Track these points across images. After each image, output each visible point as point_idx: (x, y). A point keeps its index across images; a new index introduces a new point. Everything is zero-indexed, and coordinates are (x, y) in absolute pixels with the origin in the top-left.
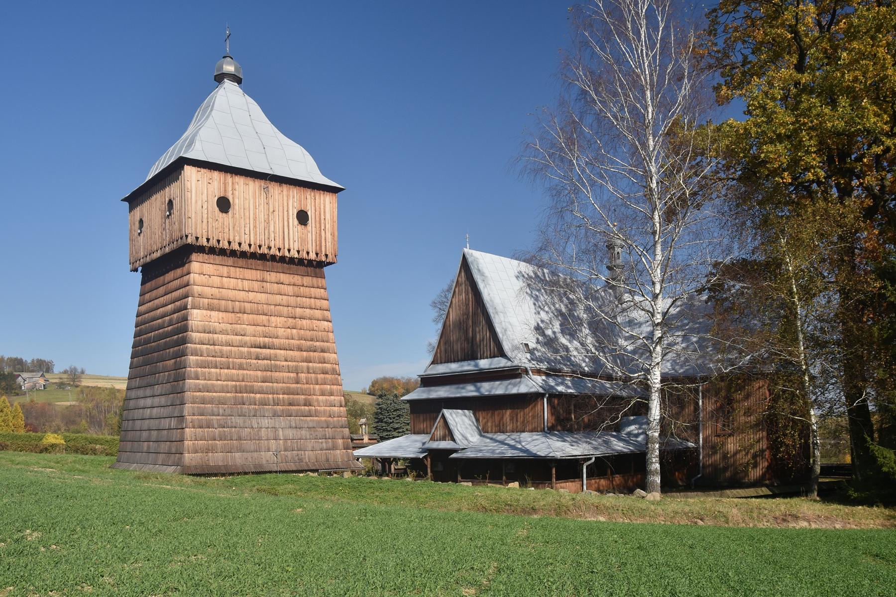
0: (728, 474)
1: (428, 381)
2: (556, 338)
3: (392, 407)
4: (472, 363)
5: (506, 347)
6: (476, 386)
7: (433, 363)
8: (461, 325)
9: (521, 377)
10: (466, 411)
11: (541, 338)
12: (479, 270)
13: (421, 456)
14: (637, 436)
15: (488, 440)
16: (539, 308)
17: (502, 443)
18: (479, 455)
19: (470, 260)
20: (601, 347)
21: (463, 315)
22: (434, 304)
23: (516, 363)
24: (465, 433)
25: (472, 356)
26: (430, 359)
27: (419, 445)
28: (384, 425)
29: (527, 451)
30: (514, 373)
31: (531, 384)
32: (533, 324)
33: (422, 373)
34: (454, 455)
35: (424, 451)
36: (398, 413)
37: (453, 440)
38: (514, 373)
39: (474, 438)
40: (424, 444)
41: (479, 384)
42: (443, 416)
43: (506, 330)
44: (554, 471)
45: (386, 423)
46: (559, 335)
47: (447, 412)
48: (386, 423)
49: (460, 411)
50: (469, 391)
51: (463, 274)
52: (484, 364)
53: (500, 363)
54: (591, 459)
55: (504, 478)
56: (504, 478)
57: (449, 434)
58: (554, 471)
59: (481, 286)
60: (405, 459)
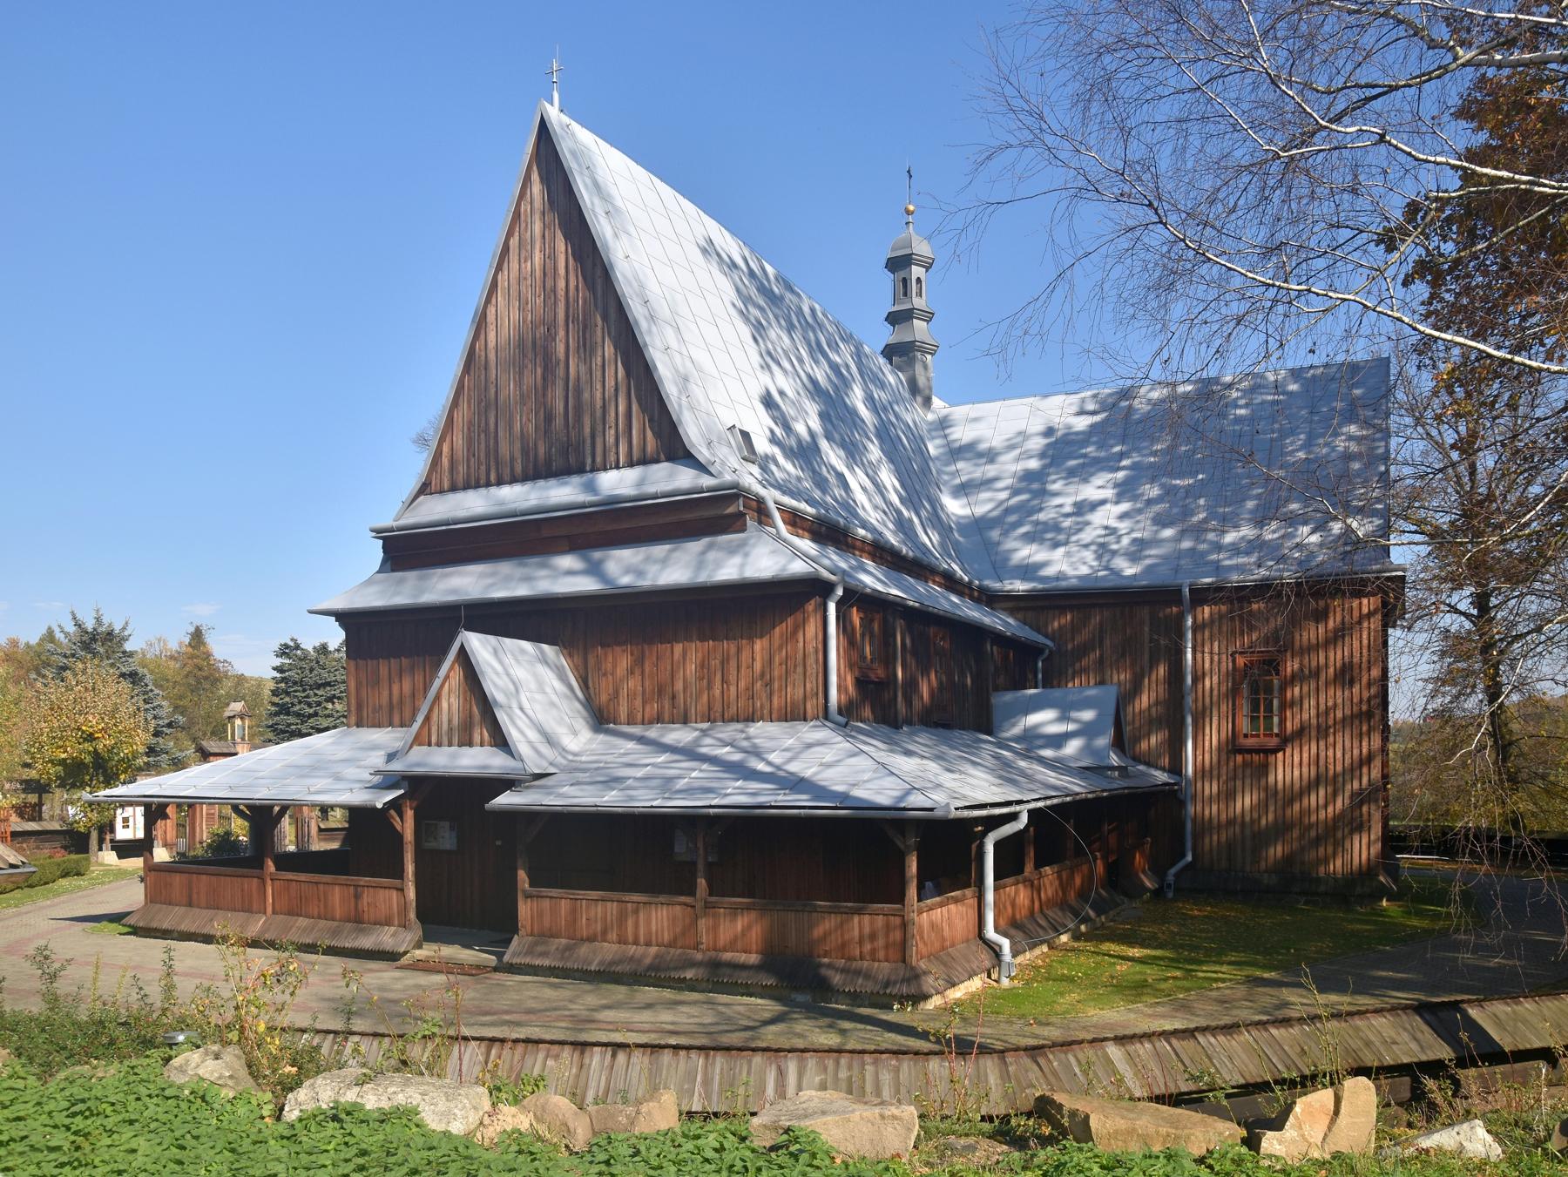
0: (1277, 851)
1: (406, 550)
2: (817, 450)
3: (311, 679)
4: (576, 480)
5: (692, 432)
6: (586, 559)
7: (425, 489)
8: (534, 348)
9: (743, 529)
10: (545, 646)
11: (778, 431)
12: (596, 184)
13: (383, 799)
14: (1058, 741)
15: (631, 745)
16: (770, 359)
17: (690, 753)
18: (610, 799)
19: (565, 148)
20: (911, 500)
21: (534, 326)
22: (422, 441)
23: (728, 478)
24: (542, 723)
25: (570, 460)
26: (416, 465)
27: (377, 760)
28: (292, 720)
29: (798, 784)
30: (720, 513)
31: (766, 557)
32: (756, 392)
33: (387, 521)
34: (505, 800)
35: (389, 781)
36: (329, 691)
37: (500, 741)
38: (720, 513)
39: (579, 739)
40: (391, 757)
41: (597, 555)
42: (464, 657)
43: (686, 379)
44: (913, 866)
45: (298, 715)
46: (824, 445)
47: (478, 644)
48: (298, 715)
49: (526, 645)
50: (564, 576)
51: (536, 188)
52: (617, 482)
53: (670, 479)
54: (1014, 817)
55: (702, 882)
56: (702, 882)
57: (483, 717)
58: (913, 866)
59: (601, 227)
60: (342, 807)
